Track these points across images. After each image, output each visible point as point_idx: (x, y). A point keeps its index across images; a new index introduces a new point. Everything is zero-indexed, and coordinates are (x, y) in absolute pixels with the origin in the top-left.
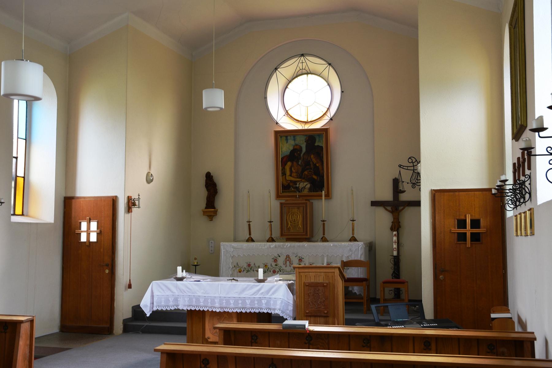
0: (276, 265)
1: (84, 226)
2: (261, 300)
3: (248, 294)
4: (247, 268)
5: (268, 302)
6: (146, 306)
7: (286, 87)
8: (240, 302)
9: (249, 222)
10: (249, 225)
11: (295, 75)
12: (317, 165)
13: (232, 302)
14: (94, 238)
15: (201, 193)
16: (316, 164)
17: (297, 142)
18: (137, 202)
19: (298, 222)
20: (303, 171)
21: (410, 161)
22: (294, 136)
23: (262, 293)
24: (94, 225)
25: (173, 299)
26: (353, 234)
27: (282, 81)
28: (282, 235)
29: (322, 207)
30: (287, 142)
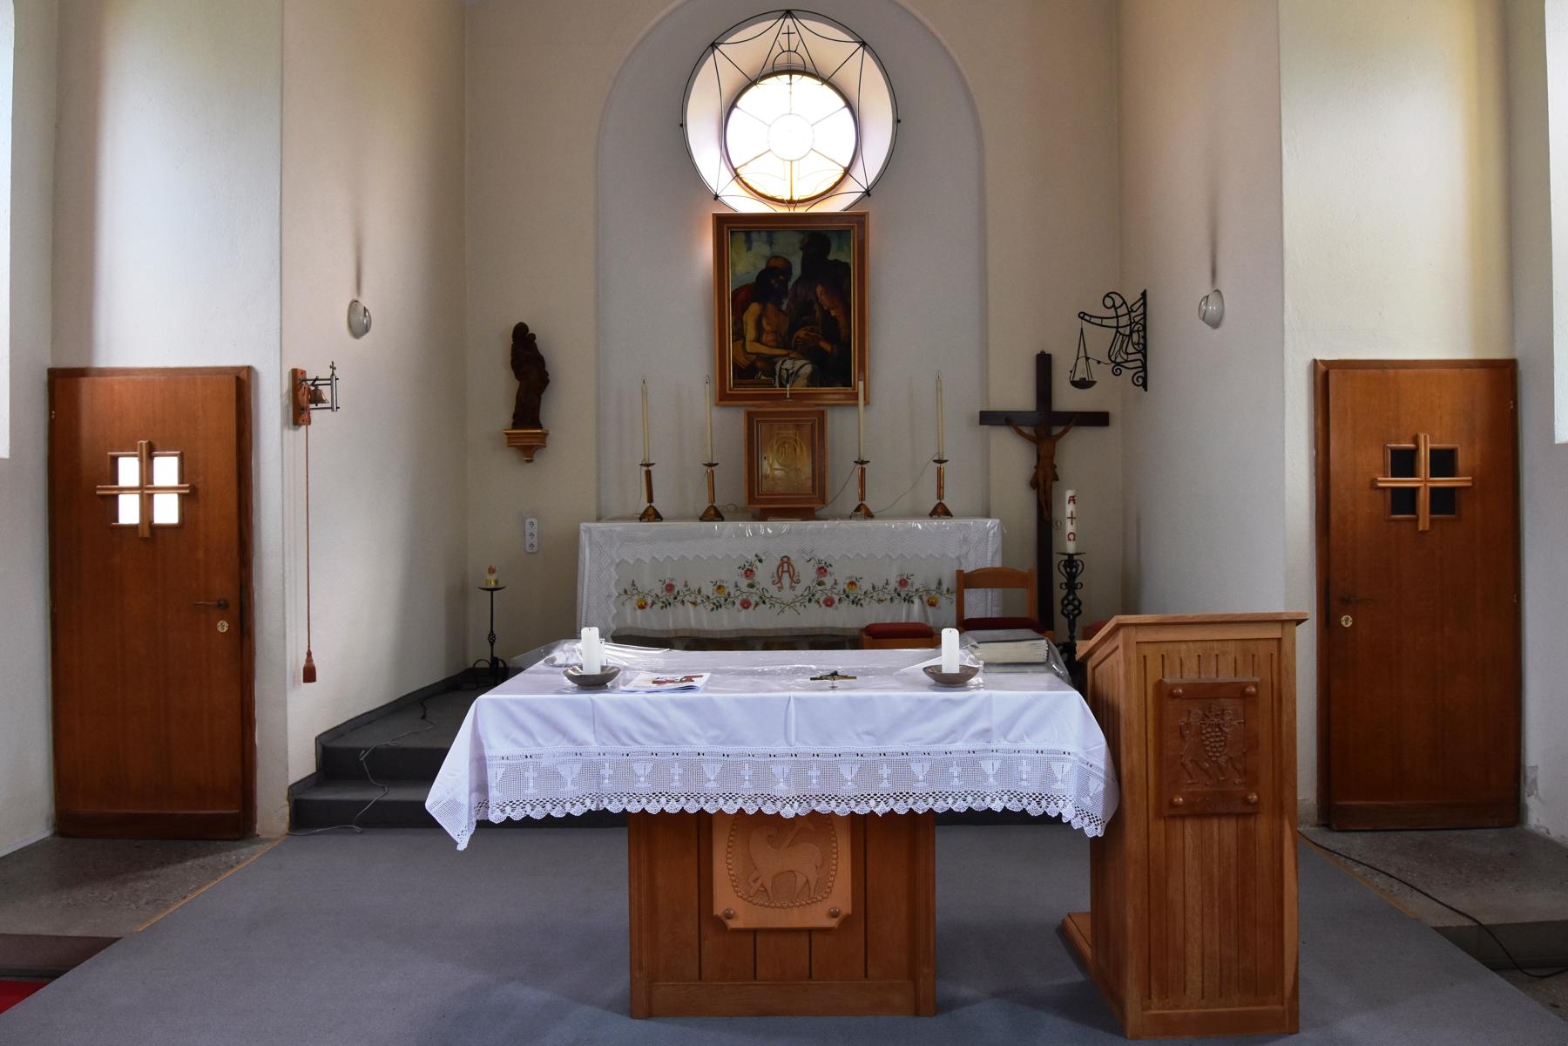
0: (751, 586)
1: (128, 470)
2: (975, 763)
4: (664, 595)
5: (1008, 768)
6: (453, 806)
7: (733, 105)
8: (885, 771)
10: (648, 474)
12: (833, 313)
13: (848, 773)
14: (167, 511)
15: (496, 387)
17: (778, 250)
18: (326, 392)
20: (793, 328)
21: (1109, 302)
22: (770, 233)
24: (167, 469)
25: (577, 768)
26: (940, 496)
27: (731, 79)
28: (751, 498)
30: (749, 249)
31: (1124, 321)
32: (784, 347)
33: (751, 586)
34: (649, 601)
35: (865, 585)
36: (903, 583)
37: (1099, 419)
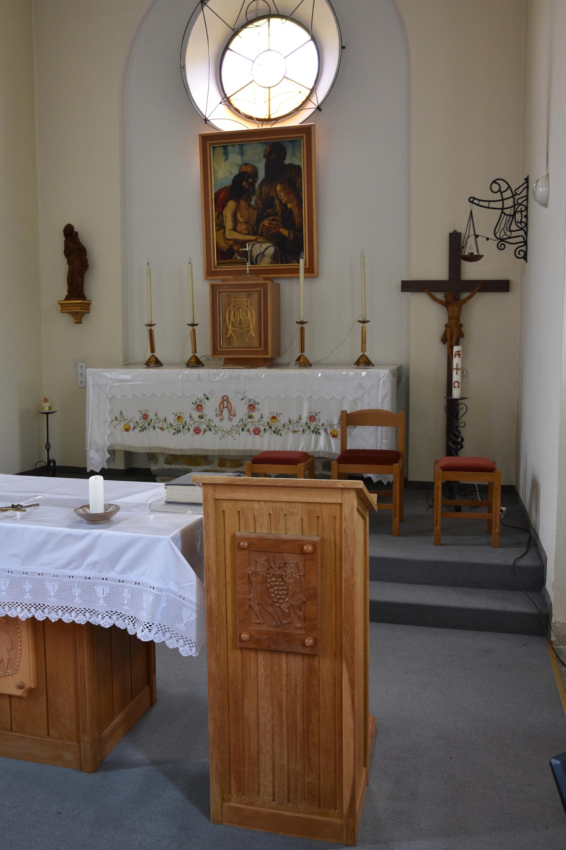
0: (201, 417)
3: (50, 561)
7: (226, 48)
8: (28, 586)
9: (151, 325)
10: (151, 332)
11: (243, 20)
12: (289, 206)
15: (57, 267)
16: (285, 205)
17: (247, 159)
19: (249, 326)
20: (260, 219)
21: (495, 187)
23: (94, 564)
26: (363, 349)
27: (218, 31)
28: (215, 351)
29: (297, 294)
30: (226, 159)
31: (509, 203)
32: (254, 234)
33: (201, 417)
34: (132, 427)
35: (283, 420)
36: (312, 418)
37: (502, 286)
